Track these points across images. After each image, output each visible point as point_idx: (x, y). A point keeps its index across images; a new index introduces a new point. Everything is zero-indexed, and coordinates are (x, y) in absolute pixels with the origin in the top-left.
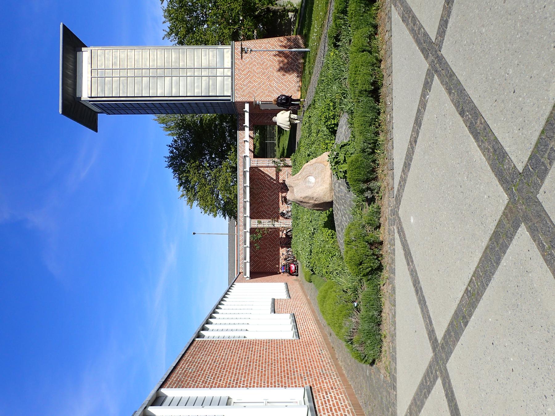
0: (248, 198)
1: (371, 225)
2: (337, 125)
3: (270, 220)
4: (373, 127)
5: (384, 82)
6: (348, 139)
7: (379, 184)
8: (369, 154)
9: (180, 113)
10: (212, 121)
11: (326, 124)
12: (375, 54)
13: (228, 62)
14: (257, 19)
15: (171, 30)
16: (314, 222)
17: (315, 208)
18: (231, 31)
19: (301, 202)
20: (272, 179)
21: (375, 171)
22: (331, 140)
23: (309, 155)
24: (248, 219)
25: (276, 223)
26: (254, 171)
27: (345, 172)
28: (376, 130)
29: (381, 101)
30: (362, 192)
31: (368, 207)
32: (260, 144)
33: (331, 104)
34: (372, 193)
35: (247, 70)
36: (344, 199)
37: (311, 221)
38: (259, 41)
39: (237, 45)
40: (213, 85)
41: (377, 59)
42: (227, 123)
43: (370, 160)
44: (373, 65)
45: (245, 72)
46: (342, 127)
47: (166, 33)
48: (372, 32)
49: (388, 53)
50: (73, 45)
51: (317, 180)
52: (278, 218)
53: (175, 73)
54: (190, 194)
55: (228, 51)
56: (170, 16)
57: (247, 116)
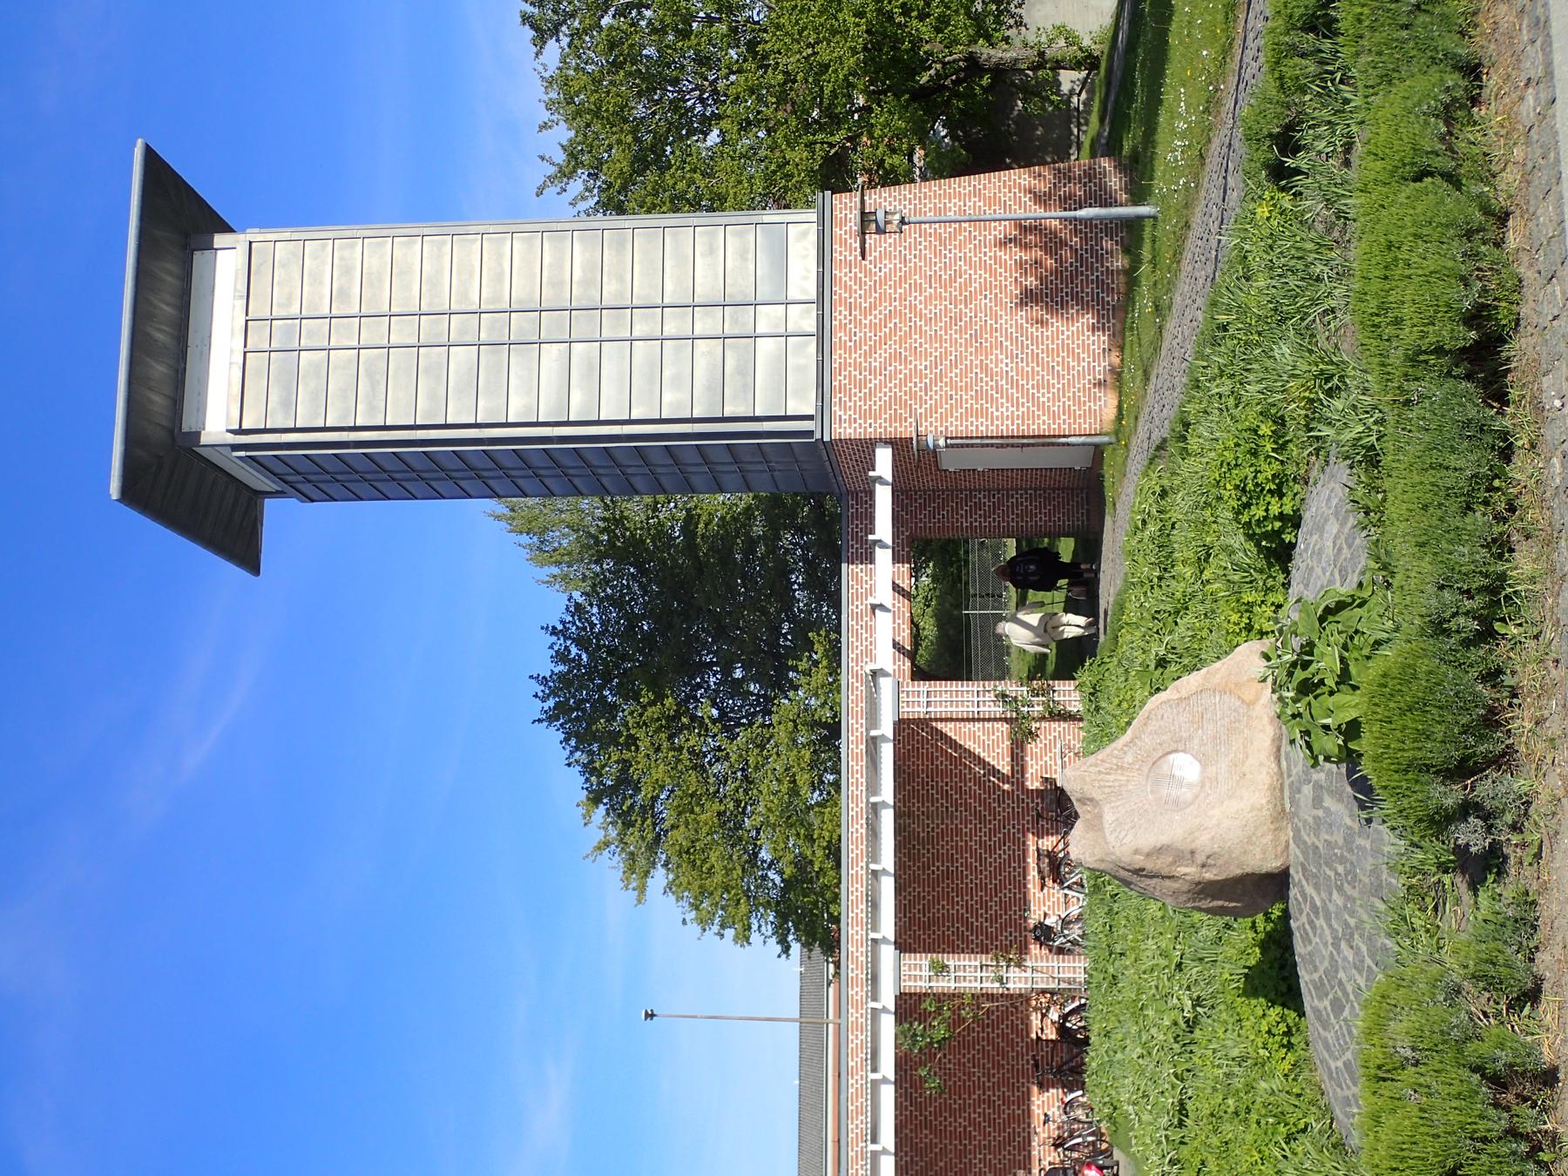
0: (887, 860)
1: (1490, 983)
2: (1294, 521)
3: (985, 959)
4: (1479, 517)
5: (1525, 310)
6: (1354, 579)
7: (1520, 784)
8: (1467, 643)
9: (601, 491)
10: (737, 524)
11: (1245, 518)
12: (1476, 188)
13: (806, 278)
14: (927, 101)
15: (572, 156)
16: (1193, 971)
17: (1206, 904)
18: (819, 154)
19: (1138, 872)
20: (994, 772)
21: (1498, 724)
22: (1268, 590)
23: (1162, 663)
24: (888, 953)
25: (1014, 973)
26: (917, 740)
27: (1352, 730)
28: (1497, 529)
29: (1514, 394)
30: (1440, 822)
31: (1467, 897)
32: (943, 620)
33: (1266, 429)
34: (1489, 829)
35: (885, 308)
36: (1342, 860)
37: (1179, 966)
38: (934, 186)
39: (845, 206)
40: (740, 371)
41: (1486, 210)
42: (800, 530)
43: (1473, 673)
44: (1469, 235)
45: (875, 317)
46: (1320, 529)
47: (552, 170)
48: (1459, 93)
49: (1541, 179)
50: (180, 222)
51: (1212, 770)
52: (1023, 949)
53: (583, 325)
54: (633, 837)
55: (805, 234)
56: (570, 101)
57: (883, 499)
